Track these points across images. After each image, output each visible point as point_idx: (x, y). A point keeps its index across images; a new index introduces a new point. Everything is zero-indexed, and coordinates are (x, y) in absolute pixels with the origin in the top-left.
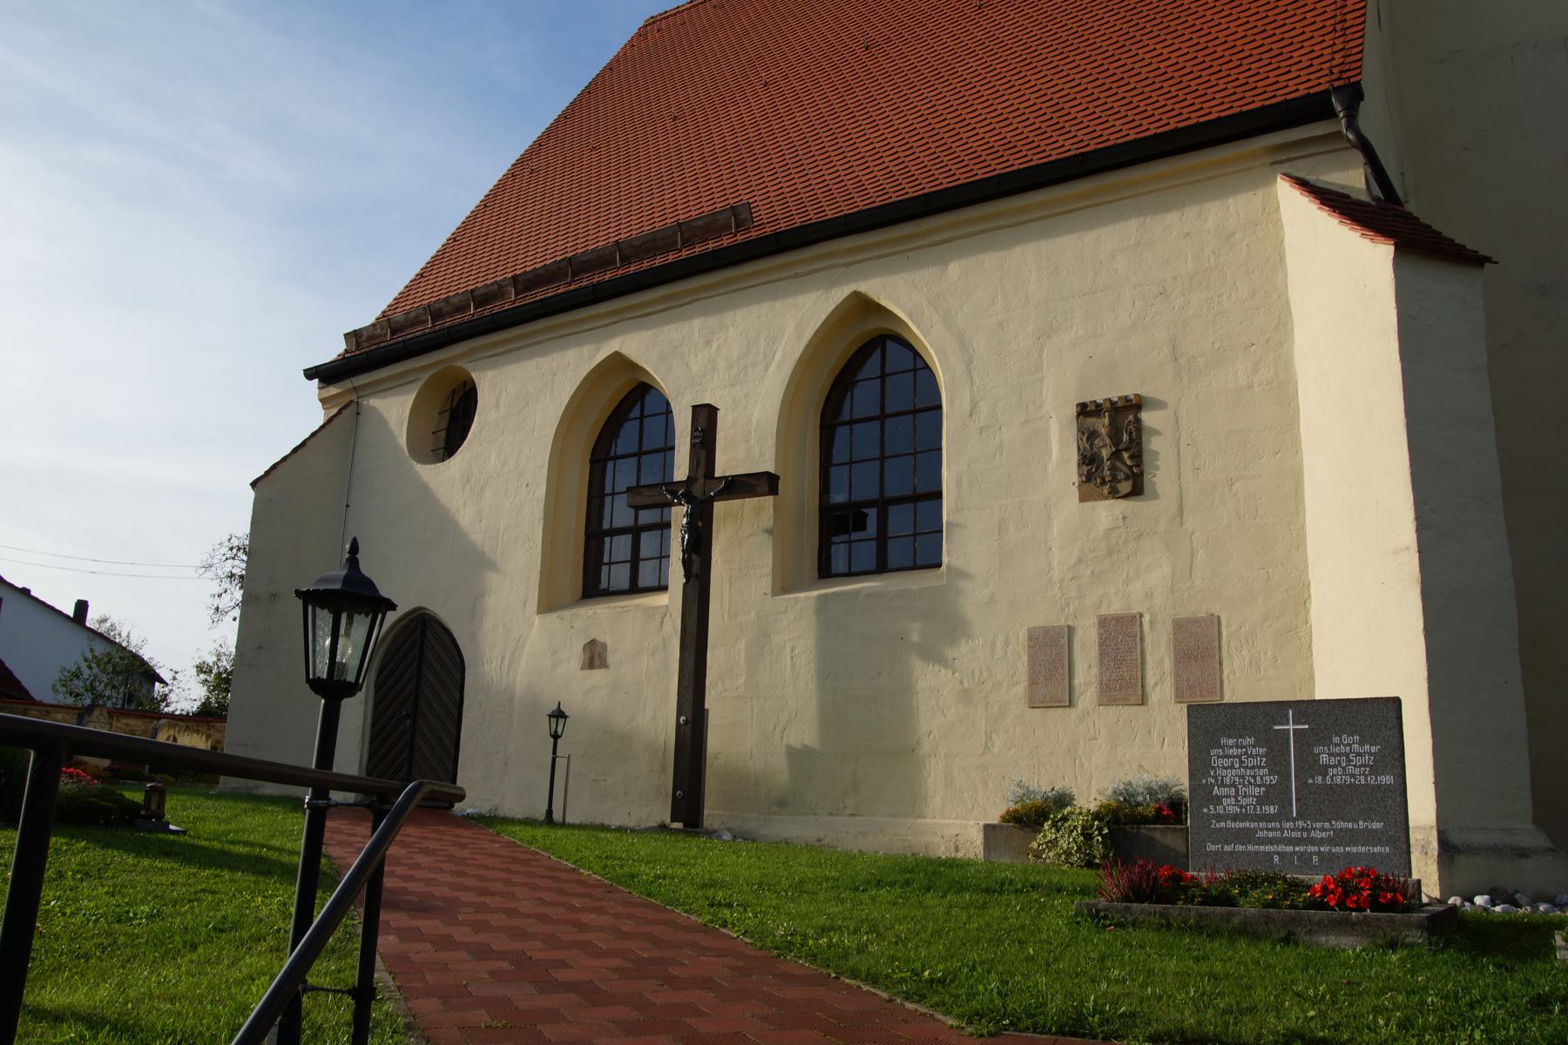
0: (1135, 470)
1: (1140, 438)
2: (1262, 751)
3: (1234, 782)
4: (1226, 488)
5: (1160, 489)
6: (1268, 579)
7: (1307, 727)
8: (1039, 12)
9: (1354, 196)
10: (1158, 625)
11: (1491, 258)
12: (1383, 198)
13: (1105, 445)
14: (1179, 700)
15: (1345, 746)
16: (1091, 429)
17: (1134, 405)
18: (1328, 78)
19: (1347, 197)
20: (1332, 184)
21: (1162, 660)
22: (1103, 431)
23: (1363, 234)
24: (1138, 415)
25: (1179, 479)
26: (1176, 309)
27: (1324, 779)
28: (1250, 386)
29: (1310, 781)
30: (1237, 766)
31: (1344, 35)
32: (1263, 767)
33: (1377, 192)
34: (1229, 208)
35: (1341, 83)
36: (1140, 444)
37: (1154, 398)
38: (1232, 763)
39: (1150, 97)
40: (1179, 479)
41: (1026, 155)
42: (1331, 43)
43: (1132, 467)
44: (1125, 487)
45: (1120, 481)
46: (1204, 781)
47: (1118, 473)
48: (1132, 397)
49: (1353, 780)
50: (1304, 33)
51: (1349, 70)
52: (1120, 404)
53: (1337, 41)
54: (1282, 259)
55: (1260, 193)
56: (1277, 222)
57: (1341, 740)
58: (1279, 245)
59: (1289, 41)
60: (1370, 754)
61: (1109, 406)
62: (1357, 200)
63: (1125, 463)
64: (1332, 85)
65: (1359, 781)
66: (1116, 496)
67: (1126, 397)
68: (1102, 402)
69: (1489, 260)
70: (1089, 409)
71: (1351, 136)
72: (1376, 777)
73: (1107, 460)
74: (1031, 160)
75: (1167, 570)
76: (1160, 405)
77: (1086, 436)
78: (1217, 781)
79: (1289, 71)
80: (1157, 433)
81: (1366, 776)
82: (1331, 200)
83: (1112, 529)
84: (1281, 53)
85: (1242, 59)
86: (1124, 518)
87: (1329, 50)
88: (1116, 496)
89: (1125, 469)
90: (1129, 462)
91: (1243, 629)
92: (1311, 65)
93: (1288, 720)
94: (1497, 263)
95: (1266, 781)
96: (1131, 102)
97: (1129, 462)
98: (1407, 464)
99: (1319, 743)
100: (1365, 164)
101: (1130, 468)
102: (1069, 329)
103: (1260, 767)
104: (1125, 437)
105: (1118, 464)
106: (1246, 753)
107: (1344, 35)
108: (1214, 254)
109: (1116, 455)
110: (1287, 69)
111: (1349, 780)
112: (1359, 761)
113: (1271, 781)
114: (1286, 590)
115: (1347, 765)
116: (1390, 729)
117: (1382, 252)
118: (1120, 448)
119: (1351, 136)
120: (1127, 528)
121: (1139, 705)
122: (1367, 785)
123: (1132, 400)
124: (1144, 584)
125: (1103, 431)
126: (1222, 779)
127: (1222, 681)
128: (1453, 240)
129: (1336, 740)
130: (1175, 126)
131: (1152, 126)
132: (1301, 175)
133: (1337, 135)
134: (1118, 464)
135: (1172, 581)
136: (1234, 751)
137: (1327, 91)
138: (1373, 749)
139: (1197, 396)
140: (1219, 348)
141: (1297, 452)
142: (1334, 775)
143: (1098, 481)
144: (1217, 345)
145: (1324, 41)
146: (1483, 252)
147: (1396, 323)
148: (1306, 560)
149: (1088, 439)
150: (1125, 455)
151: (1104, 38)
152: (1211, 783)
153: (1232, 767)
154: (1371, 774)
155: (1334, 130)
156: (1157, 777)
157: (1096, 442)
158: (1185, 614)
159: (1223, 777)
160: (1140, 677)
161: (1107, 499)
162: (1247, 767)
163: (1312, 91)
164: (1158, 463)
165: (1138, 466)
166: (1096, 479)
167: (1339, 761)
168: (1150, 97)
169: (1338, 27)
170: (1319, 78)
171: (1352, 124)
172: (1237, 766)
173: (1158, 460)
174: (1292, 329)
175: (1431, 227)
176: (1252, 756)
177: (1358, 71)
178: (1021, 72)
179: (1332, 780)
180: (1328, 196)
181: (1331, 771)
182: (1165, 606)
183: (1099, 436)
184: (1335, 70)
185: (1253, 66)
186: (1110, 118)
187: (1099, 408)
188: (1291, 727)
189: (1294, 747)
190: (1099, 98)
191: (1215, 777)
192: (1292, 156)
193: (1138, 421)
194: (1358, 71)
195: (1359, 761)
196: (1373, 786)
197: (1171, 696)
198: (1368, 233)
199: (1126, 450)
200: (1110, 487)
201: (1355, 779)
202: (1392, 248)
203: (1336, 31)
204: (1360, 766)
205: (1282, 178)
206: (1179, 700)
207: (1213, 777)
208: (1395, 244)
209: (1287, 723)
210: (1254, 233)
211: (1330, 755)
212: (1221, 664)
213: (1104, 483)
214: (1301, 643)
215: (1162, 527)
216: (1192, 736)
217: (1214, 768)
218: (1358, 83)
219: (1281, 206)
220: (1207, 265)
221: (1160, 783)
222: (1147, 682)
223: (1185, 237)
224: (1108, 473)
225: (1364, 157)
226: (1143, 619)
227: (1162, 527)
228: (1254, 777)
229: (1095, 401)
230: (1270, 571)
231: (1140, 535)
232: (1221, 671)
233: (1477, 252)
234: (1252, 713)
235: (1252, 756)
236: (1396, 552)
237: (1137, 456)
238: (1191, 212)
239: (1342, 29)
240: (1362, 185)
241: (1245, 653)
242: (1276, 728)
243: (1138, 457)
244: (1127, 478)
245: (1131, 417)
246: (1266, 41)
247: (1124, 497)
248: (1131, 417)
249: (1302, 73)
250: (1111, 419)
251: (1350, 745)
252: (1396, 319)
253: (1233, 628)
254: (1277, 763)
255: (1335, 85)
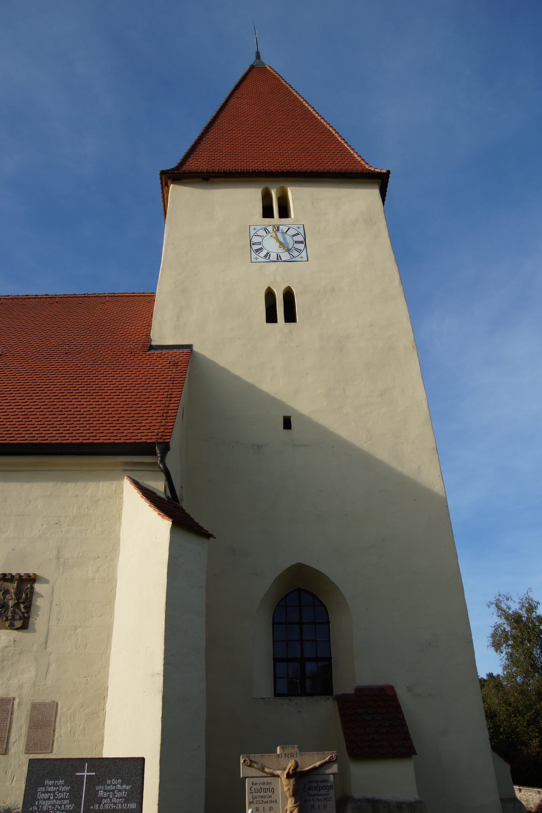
0: (26, 615)
1: (32, 597)
2: (67, 788)
3: (49, 809)
4: (73, 631)
5: (37, 627)
6: (87, 683)
7: (94, 774)
8: (25, 372)
9: (159, 494)
10: (23, 706)
11: (213, 535)
12: (171, 497)
13: (12, 599)
14: (27, 752)
15: (113, 785)
16: (6, 589)
17: (32, 579)
18: (156, 437)
19: (155, 494)
20: (149, 486)
21: (21, 727)
22: (12, 591)
23: (159, 514)
24: (33, 585)
25: (48, 623)
26: (64, 532)
27: (99, 806)
28: (94, 579)
29: (92, 807)
30: (52, 798)
31: (166, 419)
32: (67, 799)
33: (169, 494)
34: (99, 487)
35: (161, 441)
36: (31, 601)
37: (42, 577)
38: (49, 796)
39: (73, 424)
40: (48, 623)
41: (4, 437)
42: (160, 421)
43: (24, 613)
44: (18, 624)
45: (16, 620)
46: (31, 809)
47: (16, 615)
48: (32, 574)
49: (115, 807)
50: (149, 413)
51: (165, 436)
52: (24, 577)
53: (161, 427)
54: (120, 518)
55: (115, 483)
56: (121, 499)
57: (111, 782)
58: (120, 511)
59: (142, 415)
60: (126, 790)
61: (18, 578)
62: (159, 496)
63: (20, 610)
64: (157, 441)
65: (118, 807)
66: (13, 628)
67: (28, 574)
68: (15, 574)
69: (212, 536)
70: (7, 577)
71: (161, 466)
72: (127, 805)
73: (11, 607)
74: (6, 440)
75: (33, 673)
76: (45, 581)
77: (2, 592)
78: (38, 809)
79: (140, 429)
80: (41, 596)
81: (122, 804)
82: (147, 494)
83: (7, 647)
84: (159, 378)
85: (120, 417)
86: (15, 641)
87: (159, 424)
88: (13, 628)
89: (20, 614)
90: (23, 610)
91: (69, 711)
92: (150, 429)
93: (84, 770)
94: (215, 538)
95: (67, 808)
96: (63, 424)
97: (23, 610)
98: (164, 630)
99: (99, 784)
100: (166, 480)
101: (23, 613)
102: (5, 532)
103: (65, 799)
104: (24, 596)
105: (17, 610)
106: (58, 790)
107: (166, 419)
108: (88, 508)
109: (17, 605)
110: (139, 428)
111: (113, 806)
112: (119, 794)
113: (70, 808)
114: (96, 691)
115: (113, 797)
116: (137, 776)
117: (166, 524)
118: (20, 601)
119: (161, 466)
120: (15, 647)
121: (3, 754)
122: (122, 810)
123: (31, 576)
124: (19, 681)
125: (12, 591)
126: (42, 807)
127: (53, 741)
128: (198, 524)
129: (109, 782)
130: (81, 441)
131: (70, 438)
132: (136, 479)
133: (155, 464)
134: (17, 610)
135: (35, 680)
136: (52, 789)
137: (154, 444)
138: (128, 787)
139: (66, 580)
140: (81, 557)
141: (112, 616)
142: (105, 803)
143: (4, 619)
144: (80, 555)
145: (157, 419)
146: (210, 532)
147: (167, 559)
148: (108, 675)
149: (3, 594)
150: (22, 606)
151: (58, 389)
152: (35, 810)
153: (49, 799)
154: (125, 803)
155: (154, 462)
156: (4, 803)
157: (7, 596)
158: (39, 700)
159: (42, 805)
160: (6, 737)
161: (7, 629)
162: (57, 799)
163: (148, 441)
164: (39, 613)
165: (27, 613)
166: (3, 617)
167: (109, 795)
168: (73, 424)
169: (165, 415)
170: (152, 436)
171: (163, 461)
172: (52, 798)
173: (39, 611)
174: (119, 553)
175: (190, 515)
176: (61, 792)
177: (169, 437)
178: (12, 393)
179: (104, 807)
180: (147, 492)
181: (104, 801)
182: (29, 694)
183: (9, 593)
184: (160, 434)
185: (124, 422)
186: (51, 429)
187: (13, 578)
188: (86, 774)
189: (86, 786)
190: (48, 417)
191: (38, 806)
192: (133, 469)
193: (32, 588)
194: (169, 437)
195: (119, 794)
196: (125, 810)
197: (23, 749)
198: (161, 514)
199: (23, 603)
200: (10, 623)
201: (116, 806)
202: (171, 523)
203: (163, 416)
204: (120, 798)
205: (127, 478)
206: (27, 752)
207: (37, 806)
208: (172, 521)
209: (84, 772)
210: (109, 502)
211: (105, 791)
212: (54, 731)
213: (7, 620)
214: (99, 721)
215: (34, 649)
216: (29, 779)
217: (38, 800)
218: (169, 442)
219: (124, 491)
220: (83, 513)
221: (5, 808)
222: (10, 740)
223: (75, 497)
224: (10, 614)
225: (166, 477)
226: (15, 701)
227: (34, 649)
228: (60, 805)
229: (11, 574)
230: (89, 679)
231: (22, 652)
232: (54, 735)
233: (208, 532)
234: (65, 765)
235: (61, 792)
236: (153, 675)
237: (28, 607)
238: (80, 485)
239: (166, 416)
240: (163, 490)
241: (68, 725)
242: (77, 774)
243: (28, 608)
244: (20, 619)
245: (29, 586)
246: (132, 412)
247: (17, 629)
248: (29, 586)
249: (145, 431)
250: (18, 585)
251: (115, 785)
252: (168, 558)
253: (64, 710)
254: (75, 797)
255: (158, 441)
